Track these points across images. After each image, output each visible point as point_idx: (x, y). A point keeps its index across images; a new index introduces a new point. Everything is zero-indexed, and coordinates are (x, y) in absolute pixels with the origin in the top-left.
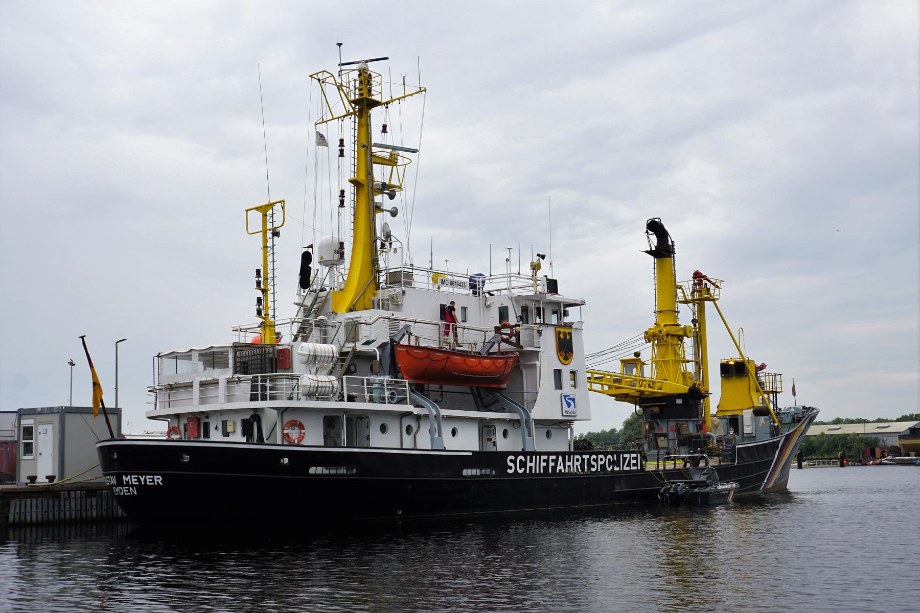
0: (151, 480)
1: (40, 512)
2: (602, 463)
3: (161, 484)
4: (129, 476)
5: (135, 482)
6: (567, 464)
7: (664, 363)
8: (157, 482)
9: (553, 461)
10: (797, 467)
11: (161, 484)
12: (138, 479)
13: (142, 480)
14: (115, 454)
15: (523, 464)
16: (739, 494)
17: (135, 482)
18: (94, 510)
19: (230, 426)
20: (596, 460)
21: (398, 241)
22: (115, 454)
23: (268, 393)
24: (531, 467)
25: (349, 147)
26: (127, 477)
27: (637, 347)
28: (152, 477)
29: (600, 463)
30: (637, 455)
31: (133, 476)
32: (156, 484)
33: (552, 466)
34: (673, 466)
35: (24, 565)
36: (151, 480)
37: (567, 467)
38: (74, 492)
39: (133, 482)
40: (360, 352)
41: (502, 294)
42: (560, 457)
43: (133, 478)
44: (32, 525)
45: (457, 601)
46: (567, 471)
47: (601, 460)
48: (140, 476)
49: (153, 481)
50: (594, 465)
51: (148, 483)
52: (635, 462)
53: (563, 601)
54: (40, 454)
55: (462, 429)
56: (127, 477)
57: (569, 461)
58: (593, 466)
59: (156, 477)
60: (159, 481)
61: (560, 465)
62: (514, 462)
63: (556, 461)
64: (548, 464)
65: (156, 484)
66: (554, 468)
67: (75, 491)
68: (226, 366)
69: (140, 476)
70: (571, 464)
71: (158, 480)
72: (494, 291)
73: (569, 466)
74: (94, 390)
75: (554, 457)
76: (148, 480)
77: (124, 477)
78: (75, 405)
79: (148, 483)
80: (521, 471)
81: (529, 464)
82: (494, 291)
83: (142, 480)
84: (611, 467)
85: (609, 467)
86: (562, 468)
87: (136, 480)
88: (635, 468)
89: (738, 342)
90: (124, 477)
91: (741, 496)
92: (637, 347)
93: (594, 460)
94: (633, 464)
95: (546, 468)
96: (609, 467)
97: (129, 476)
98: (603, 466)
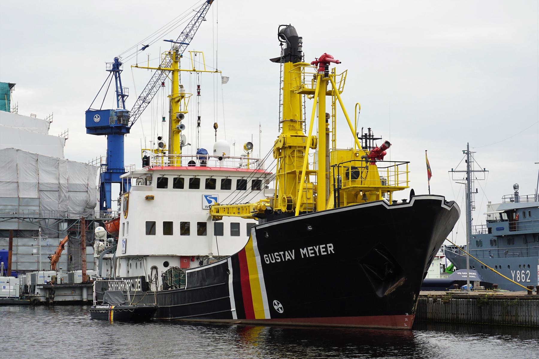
0: (324, 250)
3: (333, 252)
4: (305, 249)
10: (307, 170)
11: (333, 252)
12: (313, 249)
13: (317, 250)
14: (267, 233)
19: (59, 279)
22: (267, 233)
25: (167, 119)
26: (303, 250)
31: (309, 248)
32: (329, 253)
33: (283, 254)
35: (178, 320)
36: (324, 250)
39: (322, 252)
40: (3, 291)
43: (309, 250)
48: (314, 247)
49: (326, 251)
50: (278, 258)
51: (323, 254)
56: (303, 250)
59: (328, 245)
61: (288, 256)
65: (329, 253)
69: (314, 247)
71: (331, 248)
72: (142, 156)
76: (322, 250)
77: (301, 250)
79: (323, 254)
82: (142, 156)
83: (317, 250)
86: (289, 257)
90: (301, 250)
94: (323, 251)
97: (305, 249)
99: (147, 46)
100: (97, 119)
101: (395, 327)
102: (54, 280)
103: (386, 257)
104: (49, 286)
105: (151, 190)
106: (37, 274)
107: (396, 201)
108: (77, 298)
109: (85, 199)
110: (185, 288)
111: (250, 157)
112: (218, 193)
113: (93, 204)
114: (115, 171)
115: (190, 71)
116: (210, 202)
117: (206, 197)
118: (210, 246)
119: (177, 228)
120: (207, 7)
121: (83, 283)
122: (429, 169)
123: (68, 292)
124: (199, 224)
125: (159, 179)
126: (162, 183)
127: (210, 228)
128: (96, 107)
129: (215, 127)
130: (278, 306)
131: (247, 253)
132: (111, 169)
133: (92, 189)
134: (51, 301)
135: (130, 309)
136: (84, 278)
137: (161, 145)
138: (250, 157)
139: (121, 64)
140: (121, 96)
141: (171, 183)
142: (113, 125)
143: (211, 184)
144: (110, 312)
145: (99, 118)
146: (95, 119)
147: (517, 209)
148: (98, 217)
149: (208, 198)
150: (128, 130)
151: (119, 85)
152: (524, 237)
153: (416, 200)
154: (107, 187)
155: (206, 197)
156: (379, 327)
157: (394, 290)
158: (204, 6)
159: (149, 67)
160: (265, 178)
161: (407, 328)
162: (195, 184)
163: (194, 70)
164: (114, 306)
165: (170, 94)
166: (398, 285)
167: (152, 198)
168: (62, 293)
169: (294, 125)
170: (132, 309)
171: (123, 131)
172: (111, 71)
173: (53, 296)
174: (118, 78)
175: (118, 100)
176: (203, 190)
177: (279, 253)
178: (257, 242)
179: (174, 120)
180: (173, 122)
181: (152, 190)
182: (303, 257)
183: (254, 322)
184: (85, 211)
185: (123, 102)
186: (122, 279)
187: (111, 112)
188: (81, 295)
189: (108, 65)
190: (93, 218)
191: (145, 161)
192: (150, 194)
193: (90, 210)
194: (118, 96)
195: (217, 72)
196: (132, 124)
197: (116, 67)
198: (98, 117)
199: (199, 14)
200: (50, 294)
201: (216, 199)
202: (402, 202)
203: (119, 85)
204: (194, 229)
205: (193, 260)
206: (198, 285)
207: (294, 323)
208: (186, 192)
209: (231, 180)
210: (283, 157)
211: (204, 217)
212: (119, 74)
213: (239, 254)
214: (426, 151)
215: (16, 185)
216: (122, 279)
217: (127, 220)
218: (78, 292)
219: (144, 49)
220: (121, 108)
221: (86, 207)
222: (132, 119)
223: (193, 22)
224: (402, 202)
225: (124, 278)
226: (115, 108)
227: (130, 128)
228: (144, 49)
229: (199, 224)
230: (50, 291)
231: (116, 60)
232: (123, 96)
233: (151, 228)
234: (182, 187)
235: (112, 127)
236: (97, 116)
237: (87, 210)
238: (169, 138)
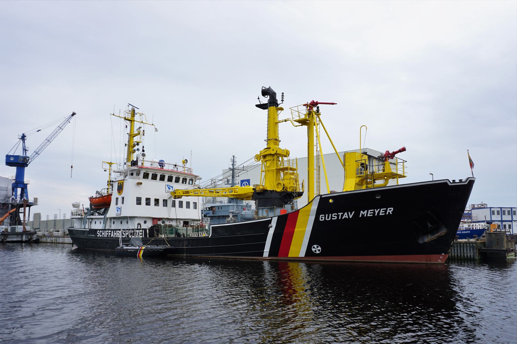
2: (127, 234)
3: (391, 213)
4: (366, 211)
6: (115, 234)
7: (268, 171)
8: (389, 213)
9: (110, 232)
11: (391, 213)
13: (377, 212)
15: (101, 234)
20: (125, 233)
24: (103, 235)
27: (219, 176)
28: (373, 210)
29: (127, 234)
30: (143, 231)
37: (114, 235)
41: (23, 220)
42: (112, 231)
44: (60, 243)
46: (114, 237)
47: (127, 233)
48: (376, 210)
52: (141, 234)
53: (45, 307)
55: (98, 222)
57: (115, 233)
58: (124, 235)
60: (390, 212)
61: (346, 216)
62: (99, 232)
63: (111, 233)
64: (108, 234)
66: (110, 235)
68: (15, 228)
69: (376, 210)
70: (116, 234)
73: (115, 235)
75: (110, 231)
78: (198, 197)
80: (101, 236)
81: (103, 234)
84: (131, 236)
85: (130, 236)
88: (141, 237)
92: (219, 176)
93: (124, 233)
95: (108, 235)
96: (130, 236)
98: (128, 235)
99: (40, 130)
100: (12, 159)
101: (429, 262)
102: (6, 230)
103: (435, 218)
104: (4, 233)
105: (139, 179)
106: (17, 227)
107: (461, 180)
108: (19, 239)
109: (6, 194)
110: (209, 237)
111: (186, 166)
112: (173, 184)
113: (10, 196)
114: (20, 183)
115: (140, 122)
116: (169, 189)
117: (168, 185)
118: (169, 212)
119: (152, 202)
120: (71, 117)
121: (23, 232)
122: (471, 162)
123: (15, 236)
124: (164, 200)
125: (144, 173)
126: (146, 176)
127: (170, 203)
128: (11, 154)
129: (72, 167)
130: (317, 249)
131: (299, 214)
132: (17, 182)
133: (9, 189)
134: (5, 241)
135: (159, 249)
136: (24, 229)
137: (143, 155)
138: (186, 166)
139: (25, 137)
140: (25, 150)
141: (150, 176)
142: (21, 162)
143: (170, 179)
144: (140, 252)
147: (215, 206)
148: (11, 202)
149: (168, 186)
150: (27, 165)
151: (24, 145)
152: (218, 217)
153: (470, 180)
154: (15, 189)
155: (168, 185)
156: (413, 262)
157: (435, 238)
158: (70, 117)
159: (120, 116)
160: (195, 178)
161: (441, 263)
162: (162, 178)
163: (142, 122)
164: (145, 247)
165: (129, 132)
166: (439, 235)
167: (141, 184)
168: (11, 236)
169: (277, 142)
170: (161, 249)
171: (25, 165)
172: (20, 139)
173: (6, 238)
174: (24, 142)
175: (23, 152)
176: (166, 182)
177: (338, 214)
178: (317, 206)
179: (131, 146)
180: (131, 147)
181: (140, 179)
182: (360, 216)
183: (438, 263)
184: (5, 199)
185: (26, 153)
186: (135, 230)
187: (20, 157)
188: (22, 238)
189: (19, 136)
190: (9, 202)
191: (133, 163)
192: (140, 181)
193: (8, 199)
194: (23, 150)
195: (153, 125)
196: (30, 163)
197: (23, 137)
198: (13, 158)
199: (67, 120)
200: (4, 237)
201: (172, 187)
202: (459, 181)
203: (24, 145)
204: (161, 203)
205: (159, 220)
206: (227, 234)
207: (327, 260)
208: (158, 183)
209: (180, 178)
210: (271, 160)
211: (166, 196)
212: (24, 141)
213: (289, 214)
214: (468, 150)
215: (103, 163)
216: (135, 230)
217: (122, 196)
218: (20, 236)
219: (38, 131)
220: (24, 155)
221: (6, 198)
222: (30, 161)
223: (64, 123)
224: (459, 181)
225: (136, 230)
226: (22, 155)
227: (28, 165)
228: (38, 131)
229: (164, 200)
230: (5, 236)
231: (23, 134)
232: (26, 150)
233: (139, 201)
234: (156, 179)
235: (20, 163)
236: (245, 184)
237: (6, 199)
238: (128, 156)
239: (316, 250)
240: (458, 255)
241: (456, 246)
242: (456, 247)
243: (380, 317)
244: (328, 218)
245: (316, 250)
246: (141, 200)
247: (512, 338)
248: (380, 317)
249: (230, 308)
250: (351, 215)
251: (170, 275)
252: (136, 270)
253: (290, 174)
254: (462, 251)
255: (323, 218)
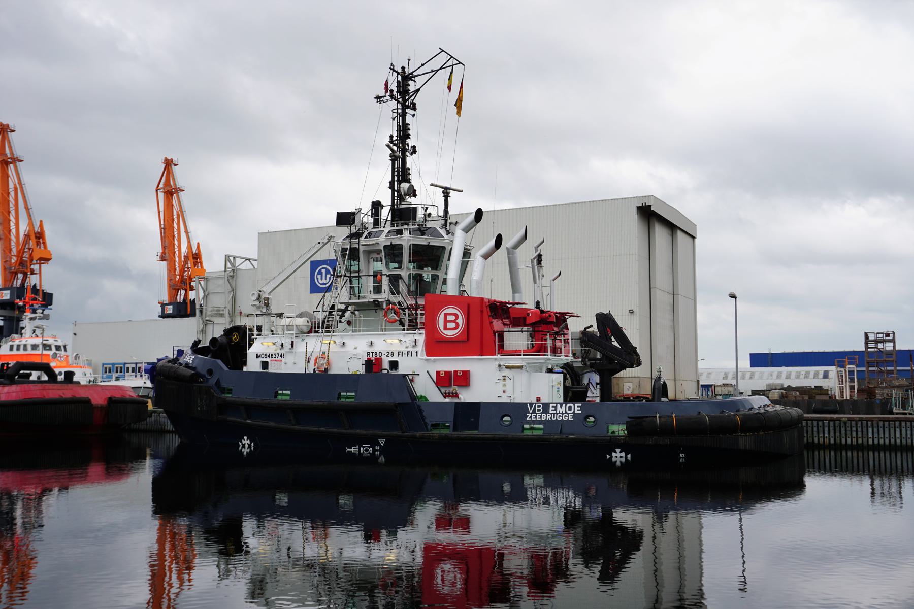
0: (554, 408)
1: (892, 438)
5: (578, 410)
16: (141, 399)
17: (578, 410)
18: (892, 438)
21: (460, 63)
23: (407, 270)
28: (869, 350)
34: (693, 382)
36: (554, 408)
38: (893, 423)
45: (367, 571)
54: (286, 363)
67: (867, 421)
74: (186, 235)
76: (533, 417)
87: (579, 408)
89: (427, 195)
91: (143, 400)
145: (328, 276)
146: (319, 276)
236: (323, 271)
239: (620, 453)
240: (908, 441)
241: (893, 426)
242: (893, 428)
243: (225, 551)
244: (554, 418)
245: (620, 453)
246: (402, 250)
247: (443, 559)
248: (225, 551)
249: (340, 589)
250: (531, 409)
251: (28, 540)
252: (533, 493)
253: (521, 350)
254: (892, 435)
255: (545, 417)
